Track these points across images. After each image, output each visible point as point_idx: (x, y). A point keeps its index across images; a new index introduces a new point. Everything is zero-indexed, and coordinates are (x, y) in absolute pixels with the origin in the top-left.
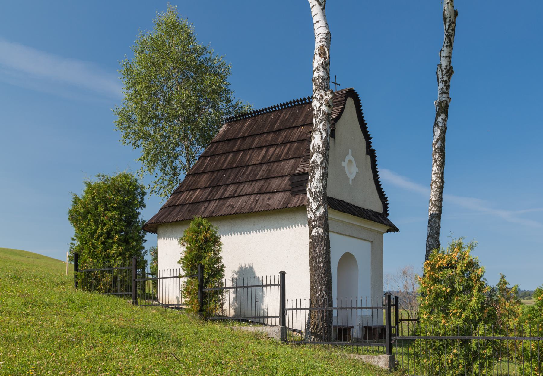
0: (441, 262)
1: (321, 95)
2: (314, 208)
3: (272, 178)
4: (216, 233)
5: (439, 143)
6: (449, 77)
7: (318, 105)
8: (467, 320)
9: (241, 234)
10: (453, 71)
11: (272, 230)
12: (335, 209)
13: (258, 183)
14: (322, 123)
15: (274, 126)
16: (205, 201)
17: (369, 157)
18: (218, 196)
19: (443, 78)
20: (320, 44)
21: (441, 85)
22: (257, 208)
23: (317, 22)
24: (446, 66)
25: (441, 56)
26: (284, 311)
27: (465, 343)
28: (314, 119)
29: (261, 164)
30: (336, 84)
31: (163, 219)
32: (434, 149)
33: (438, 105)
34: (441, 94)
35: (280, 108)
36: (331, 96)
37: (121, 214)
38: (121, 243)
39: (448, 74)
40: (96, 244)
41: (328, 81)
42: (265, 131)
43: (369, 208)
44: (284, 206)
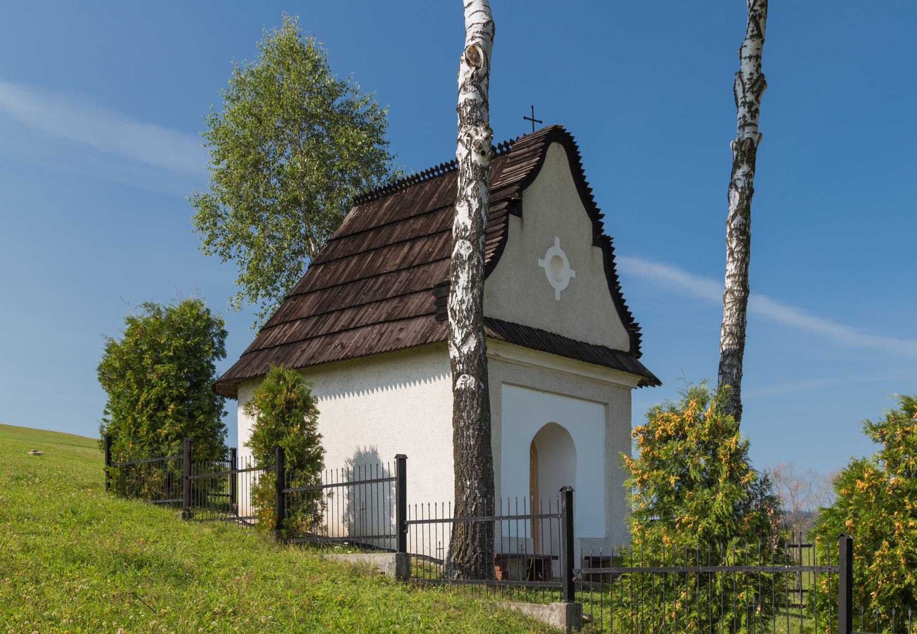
0: (662, 427)
1: (469, 135)
2: (458, 341)
3: (411, 293)
4: (309, 392)
5: (739, 218)
6: (758, 94)
7: (465, 152)
8: (707, 533)
9: (359, 395)
10: (764, 82)
11: (408, 384)
12: (519, 344)
13: (389, 304)
14: (472, 186)
15: (427, 204)
16: (305, 340)
17: (599, 251)
18: (324, 330)
19: (745, 97)
20: (471, 43)
21: (743, 111)
22: (381, 348)
23: (470, 4)
24: (751, 74)
25: (741, 58)
26: (403, 525)
27: (704, 580)
28: (459, 179)
29: (398, 271)
30: (533, 120)
31: (238, 373)
32: (728, 230)
33: (736, 149)
34: (742, 127)
35: (441, 172)
36: (485, 134)
37: (180, 368)
38: (180, 417)
39: (755, 89)
40: (139, 420)
41: (484, 108)
42: (412, 214)
43: (600, 343)
44: (422, 342)
